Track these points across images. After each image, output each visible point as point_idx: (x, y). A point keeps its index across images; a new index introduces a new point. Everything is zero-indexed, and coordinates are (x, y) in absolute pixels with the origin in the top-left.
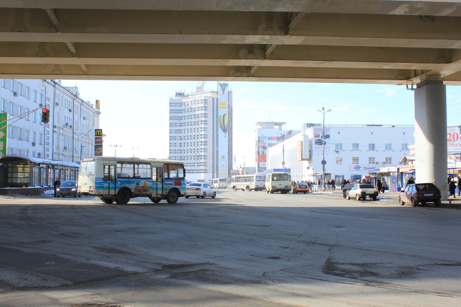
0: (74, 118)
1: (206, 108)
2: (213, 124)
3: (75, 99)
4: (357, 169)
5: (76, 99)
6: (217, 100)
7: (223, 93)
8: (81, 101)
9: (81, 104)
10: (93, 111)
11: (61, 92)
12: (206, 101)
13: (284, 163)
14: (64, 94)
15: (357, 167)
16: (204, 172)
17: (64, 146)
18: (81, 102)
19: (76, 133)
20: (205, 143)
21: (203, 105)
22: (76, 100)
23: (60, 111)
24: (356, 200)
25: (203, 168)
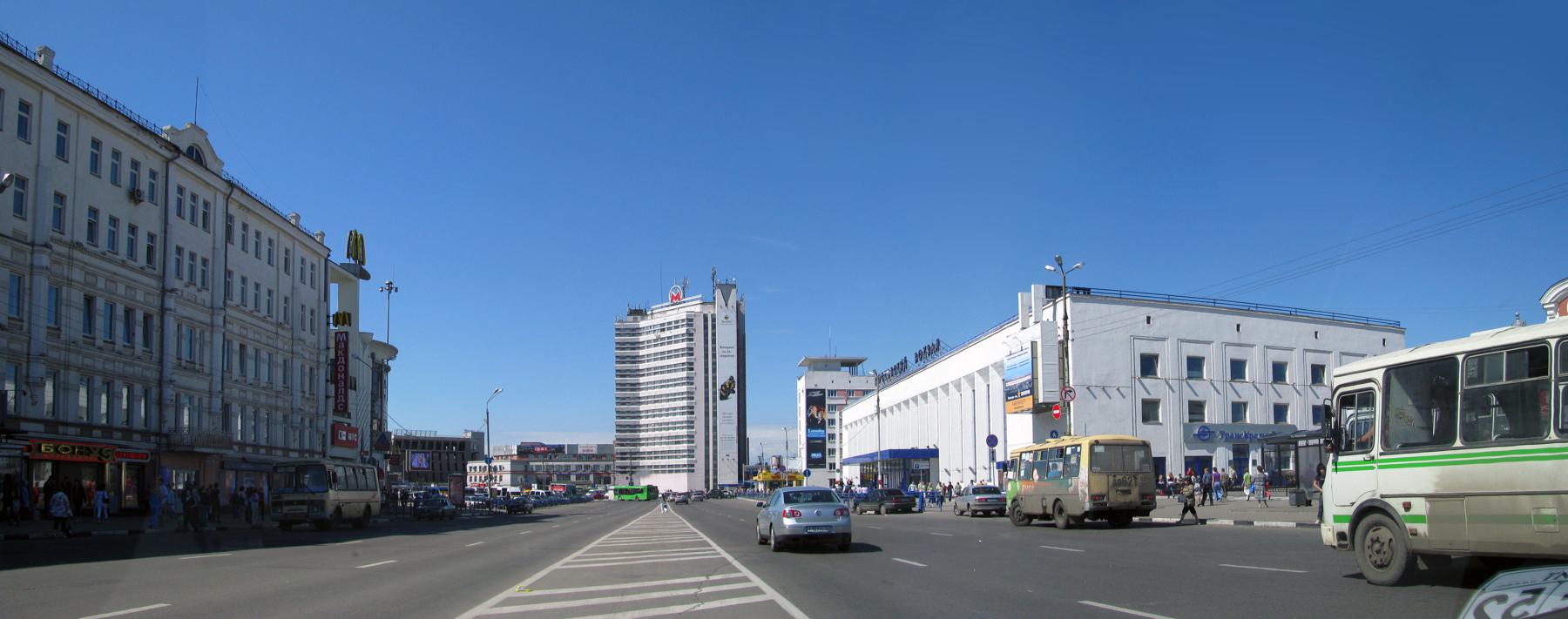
0: (165, 232)
1: (690, 336)
2: (707, 400)
3: (172, 160)
4: (1202, 437)
5: (177, 161)
6: (714, 320)
7: (726, 305)
8: (226, 185)
9: (229, 196)
10: (322, 253)
11: (297, 243)
12: (689, 321)
13: (1072, 394)
14: (78, 117)
15: (1203, 431)
16: (689, 471)
17: (392, 416)
18: (223, 187)
19: (173, 290)
20: (691, 438)
21: (683, 330)
22: (177, 165)
23: (292, 294)
24: (1054, 526)
25: (684, 446)
